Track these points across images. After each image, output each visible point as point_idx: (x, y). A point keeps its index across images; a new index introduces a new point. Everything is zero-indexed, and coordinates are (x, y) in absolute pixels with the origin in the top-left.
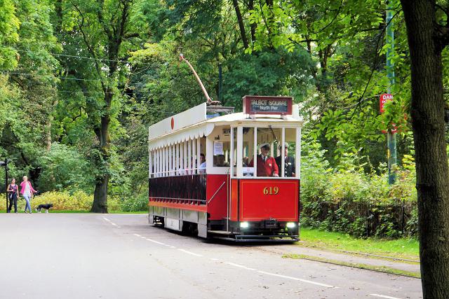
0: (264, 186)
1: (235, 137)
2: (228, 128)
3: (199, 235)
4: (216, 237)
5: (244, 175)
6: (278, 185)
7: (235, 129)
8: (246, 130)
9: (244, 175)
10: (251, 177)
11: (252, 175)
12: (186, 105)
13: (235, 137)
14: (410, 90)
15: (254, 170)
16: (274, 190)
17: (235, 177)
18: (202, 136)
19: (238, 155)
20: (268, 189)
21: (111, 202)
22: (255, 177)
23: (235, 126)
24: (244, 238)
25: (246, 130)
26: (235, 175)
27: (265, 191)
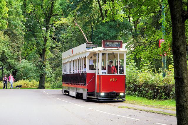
0: (111, 78)
1: (98, 57)
2: (95, 53)
3: (83, 98)
4: (91, 99)
5: (102, 73)
6: (117, 78)
7: (99, 54)
8: (103, 54)
9: (102, 73)
10: (105, 74)
11: (106, 73)
12: (78, 44)
13: (98, 57)
14: (172, 38)
15: (106, 71)
16: (115, 79)
17: (98, 74)
18: (84, 57)
19: (99, 65)
20: (112, 79)
21: (46, 84)
22: (107, 74)
23: (98, 53)
24: (102, 100)
25: (103, 54)
26: (98, 73)
27: (111, 80)
